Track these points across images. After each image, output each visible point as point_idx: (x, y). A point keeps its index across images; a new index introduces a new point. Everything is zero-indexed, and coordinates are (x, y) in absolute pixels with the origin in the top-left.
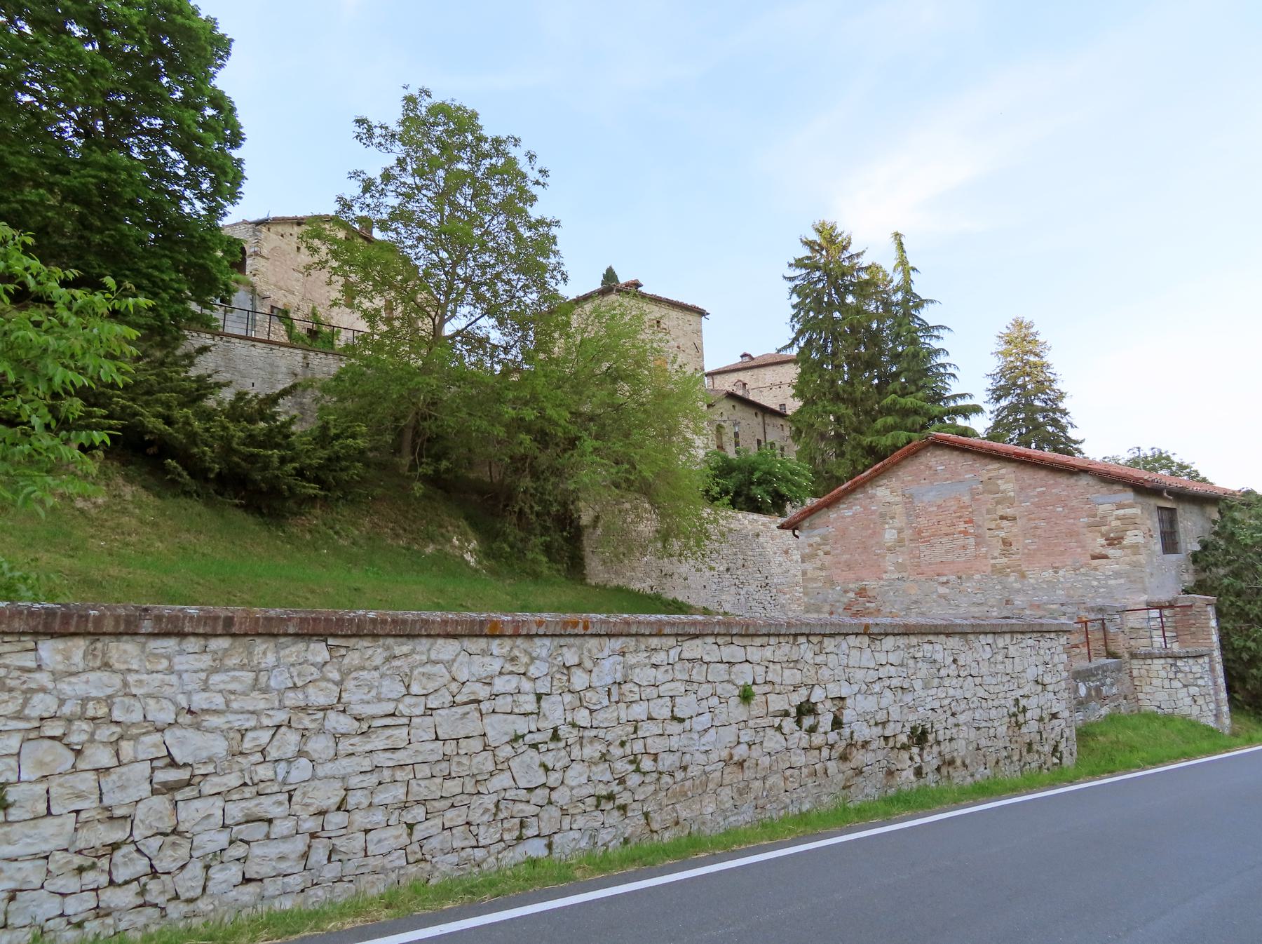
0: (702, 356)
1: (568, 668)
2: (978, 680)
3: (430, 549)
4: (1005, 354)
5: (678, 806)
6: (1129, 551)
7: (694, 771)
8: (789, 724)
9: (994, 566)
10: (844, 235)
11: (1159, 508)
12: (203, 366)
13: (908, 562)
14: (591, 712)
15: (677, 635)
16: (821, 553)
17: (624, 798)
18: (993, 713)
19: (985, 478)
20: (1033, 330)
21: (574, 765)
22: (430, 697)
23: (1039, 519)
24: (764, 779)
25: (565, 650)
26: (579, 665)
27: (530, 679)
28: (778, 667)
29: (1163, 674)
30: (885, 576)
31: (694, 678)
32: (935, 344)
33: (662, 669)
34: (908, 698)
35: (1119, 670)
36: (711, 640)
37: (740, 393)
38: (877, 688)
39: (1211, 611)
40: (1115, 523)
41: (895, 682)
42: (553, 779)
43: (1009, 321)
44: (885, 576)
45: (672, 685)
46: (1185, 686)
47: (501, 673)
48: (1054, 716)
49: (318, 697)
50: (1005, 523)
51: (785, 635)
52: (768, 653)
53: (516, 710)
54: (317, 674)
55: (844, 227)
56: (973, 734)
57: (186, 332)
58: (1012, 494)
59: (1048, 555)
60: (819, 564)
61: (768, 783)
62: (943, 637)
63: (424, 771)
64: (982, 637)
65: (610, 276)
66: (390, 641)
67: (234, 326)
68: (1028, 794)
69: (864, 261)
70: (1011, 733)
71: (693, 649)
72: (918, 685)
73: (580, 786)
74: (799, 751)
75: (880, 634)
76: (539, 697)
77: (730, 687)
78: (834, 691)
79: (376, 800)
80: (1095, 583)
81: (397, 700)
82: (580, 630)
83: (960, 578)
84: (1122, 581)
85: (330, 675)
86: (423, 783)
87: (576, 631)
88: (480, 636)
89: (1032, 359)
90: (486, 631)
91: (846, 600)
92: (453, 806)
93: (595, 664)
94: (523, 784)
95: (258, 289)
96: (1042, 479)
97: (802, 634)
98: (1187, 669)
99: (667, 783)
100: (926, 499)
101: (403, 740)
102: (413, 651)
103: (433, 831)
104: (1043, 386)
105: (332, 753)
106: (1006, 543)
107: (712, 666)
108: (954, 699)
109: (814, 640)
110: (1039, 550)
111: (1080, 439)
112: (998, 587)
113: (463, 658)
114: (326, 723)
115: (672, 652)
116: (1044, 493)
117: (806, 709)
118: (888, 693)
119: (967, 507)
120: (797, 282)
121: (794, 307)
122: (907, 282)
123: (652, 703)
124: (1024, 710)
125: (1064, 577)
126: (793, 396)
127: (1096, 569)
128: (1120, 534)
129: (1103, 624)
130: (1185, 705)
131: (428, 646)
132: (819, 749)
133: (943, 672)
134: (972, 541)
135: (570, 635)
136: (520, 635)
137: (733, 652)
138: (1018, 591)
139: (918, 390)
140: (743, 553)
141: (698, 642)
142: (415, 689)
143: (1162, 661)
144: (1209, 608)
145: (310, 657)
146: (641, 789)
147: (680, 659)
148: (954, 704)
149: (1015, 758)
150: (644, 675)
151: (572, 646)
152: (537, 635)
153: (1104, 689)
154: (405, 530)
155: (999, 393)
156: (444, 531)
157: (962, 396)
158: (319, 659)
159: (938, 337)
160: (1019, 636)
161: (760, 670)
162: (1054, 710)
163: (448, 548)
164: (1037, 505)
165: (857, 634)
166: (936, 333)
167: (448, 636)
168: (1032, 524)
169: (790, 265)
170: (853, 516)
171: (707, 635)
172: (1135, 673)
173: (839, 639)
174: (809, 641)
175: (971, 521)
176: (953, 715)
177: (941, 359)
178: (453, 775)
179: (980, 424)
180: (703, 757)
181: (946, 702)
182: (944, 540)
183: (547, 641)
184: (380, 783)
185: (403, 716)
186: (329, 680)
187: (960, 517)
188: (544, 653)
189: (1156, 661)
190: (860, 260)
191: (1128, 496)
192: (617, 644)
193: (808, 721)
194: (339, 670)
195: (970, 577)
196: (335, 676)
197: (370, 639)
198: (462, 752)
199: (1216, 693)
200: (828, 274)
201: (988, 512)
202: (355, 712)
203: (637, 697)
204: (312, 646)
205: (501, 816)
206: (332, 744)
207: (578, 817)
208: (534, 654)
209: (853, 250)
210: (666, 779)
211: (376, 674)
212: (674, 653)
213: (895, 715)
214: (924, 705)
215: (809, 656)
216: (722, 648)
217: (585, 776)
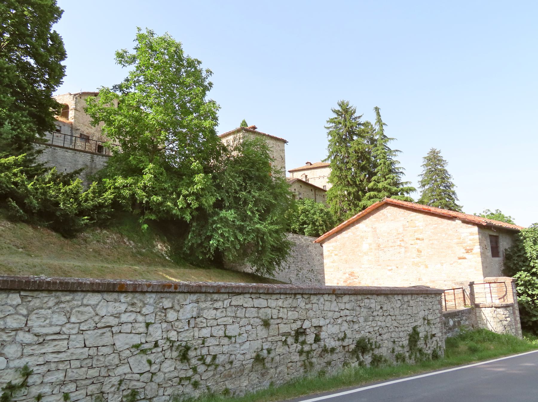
0: (284, 161)
1: (166, 309)
2: (393, 318)
4: (426, 165)
5: (226, 382)
7: (237, 364)
8: (290, 340)
10: (352, 108)
11: (490, 236)
12: (41, 159)
14: (178, 333)
15: (228, 293)
16: (333, 255)
17: (197, 377)
18: (402, 334)
21: (166, 361)
22: (82, 324)
24: (276, 368)
25: (164, 300)
26: (172, 308)
27: (143, 315)
28: (285, 310)
31: (238, 315)
32: (394, 159)
33: (220, 311)
34: (356, 327)
36: (248, 296)
37: (304, 180)
41: (349, 318)
42: (154, 368)
45: (225, 319)
47: (125, 311)
48: (434, 335)
49: (12, 323)
50: (418, 241)
51: (289, 294)
52: (280, 303)
53: (134, 331)
54: (12, 311)
55: (352, 104)
58: (421, 228)
61: (279, 370)
62: (375, 296)
63: (77, 364)
64: (395, 296)
65: (244, 123)
66: (59, 294)
68: (468, 364)
69: (362, 120)
71: (237, 300)
72: (361, 320)
73: (169, 372)
74: (296, 354)
75: (341, 294)
76: (148, 325)
77: (258, 320)
78: (316, 322)
79: (46, 380)
81: (62, 326)
82: (172, 289)
85: (21, 311)
86: (75, 371)
87: (170, 290)
88: (113, 292)
90: (117, 289)
92: (93, 383)
93: (181, 307)
94: (136, 371)
97: (299, 294)
99: (221, 370)
101: (64, 347)
102: (73, 299)
103: (79, 397)
105: (19, 354)
106: (419, 251)
107: (248, 309)
108: (380, 327)
109: (306, 296)
111: (461, 205)
113: (103, 303)
114: (17, 338)
115: (226, 302)
117: (300, 333)
118: (345, 324)
120: (331, 130)
123: (213, 328)
126: (328, 182)
127: (460, 264)
131: (82, 297)
133: (375, 314)
134: (403, 250)
135: (167, 292)
136: (137, 292)
137: (261, 302)
140: (301, 255)
141: (241, 297)
142: (73, 319)
145: (9, 302)
146: (205, 374)
147: (230, 305)
148: (380, 329)
150: (210, 314)
151: (168, 298)
152: (147, 292)
153: (462, 322)
157: (406, 183)
158: (15, 303)
160: (416, 296)
161: (275, 311)
162: (433, 333)
165: (329, 294)
166: (394, 154)
167: (94, 291)
168: (431, 242)
169: (328, 122)
171: (246, 293)
173: (319, 296)
174: (303, 297)
175: (403, 240)
176: (380, 335)
178: (94, 366)
179: (416, 196)
180: (242, 356)
181: (377, 328)
183: (154, 295)
184: (49, 371)
185: (65, 334)
186: (20, 314)
187: (398, 238)
188: (152, 301)
192: (194, 297)
193: (301, 339)
194: (27, 309)
196: (25, 312)
197: (47, 292)
198: (100, 354)
199: (515, 325)
202: (35, 332)
203: (205, 325)
204: (11, 295)
205: (122, 388)
206: (20, 349)
207: (168, 389)
208: (146, 302)
209: (356, 115)
210: (221, 368)
211: (50, 311)
212: (227, 303)
213: (349, 335)
214: (365, 330)
215: (302, 305)
216: (254, 300)
217: (173, 367)
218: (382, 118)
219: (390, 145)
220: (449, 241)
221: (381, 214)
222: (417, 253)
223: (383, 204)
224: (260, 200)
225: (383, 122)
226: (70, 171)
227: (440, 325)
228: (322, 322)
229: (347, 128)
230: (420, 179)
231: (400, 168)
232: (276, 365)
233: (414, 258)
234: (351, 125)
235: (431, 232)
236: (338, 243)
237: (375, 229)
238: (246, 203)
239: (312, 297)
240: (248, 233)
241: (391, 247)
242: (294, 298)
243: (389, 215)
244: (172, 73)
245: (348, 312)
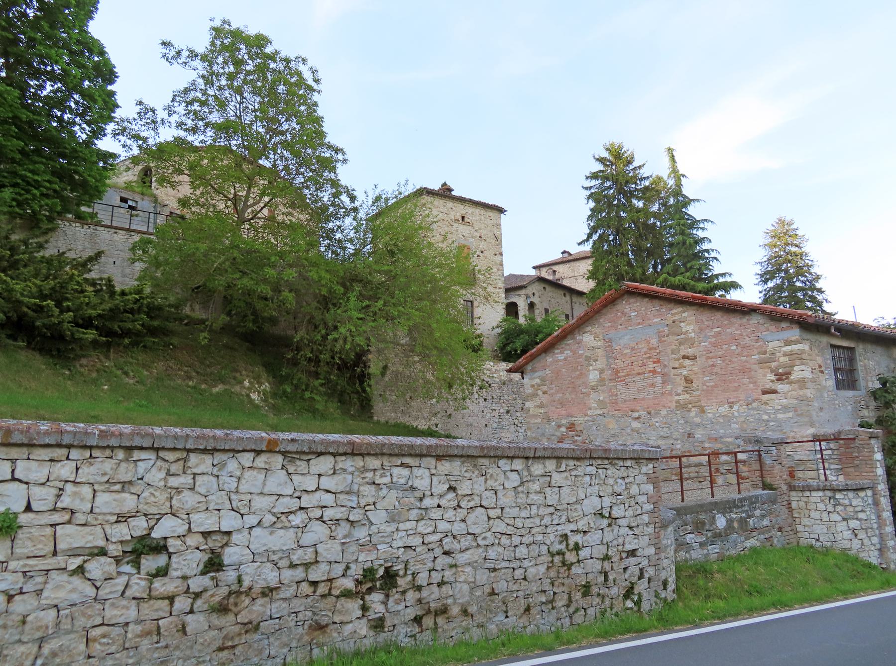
0: (500, 244)
3: (218, 389)
4: (772, 246)
6: (796, 386)
9: (677, 402)
10: (629, 153)
11: (833, 346)
13: (607, 400)
16: (540, 393)
19: (670, 322)
20: (793, 227)
23: (716, 357)
29: (821, 506)
30: (589, 412)
32: (701, 234)
34: (361, 533)
35: (774, 502)
38: (297, 519)
39: (876, 444)
40: (783, 359)
41: (328, 514)
43: (773, 220)
44: (589, 412)
46: (844, 519)
50: (687, 362)
52: (65, 470)
55: (628, 147)
56: (483, 577)
57: (60, 222)
58: (693, 335)
59: (724, 391)
60: (538, 402)
64: (502, 462)
67: (104, 216)
70: (553, 574)
78: (204, 521)
80: (765, 417)
83: (649, 413)
84: (790, 415)
89: (793, 249)
91: (559, 434)
95: (160, 199)
96: (718, 320)
98: (847, 502)
100: (622, 342)
104: (801, 271)
106: (688, 380)
110: (716, 386)
111: (834, 312)
112: (682, 421)
116: (719, 332)
119: (655, 349)
120: (593, 191)
121: (591, 210)
122: (679, 185)
124: (577, 547)
125: (738, 411)
127: (766, 403)
128: (787, 370)
129: (760, 455)
130: (844, 538)
132: (171, 599)
134: (659, 379)
138: (698, 425)
139: (687, 271)
143: (821, 494)
144: (873, 441)
149: (560, 602)
153: (751, 521)
154: (198, 373)
155: (766, 277)
156: (238, 375)
157: (723, 275)
159: (703, 229)
160: (571, 463)
162: (629, 547)
163: (237, 389)
164: (714, 345)
166: (701, 225)
168: (710, 362)
169: (587, 178)
170: (565, 360)
172: (794, 505)
173: (219, 457)
175: (659, 361)
176: (446, 553)
177: (705, 246)
182: (637, 378)
187: (649, 358)
189: (814, 494)
190: (642, 171)
191: (795, 333)
195: (658, 413)
200: (615, 182)
201: (673, 353)
209: (635, 164)
214: (390, 539)
215: (156, 476)
220: (744, 358)
222: (685, 384)
226: (86, 255)
227: (650, 530)
228: (229, 522)
230: (758, 269)
231: (713, 250)
232: (39, 634)
233: (679, 395)
235: (710, 343)
236: (548, 372)
239: (194, 458)
241: (639, 374)
242: (127, 460)
244: (259, 86)
245: (328, 499)
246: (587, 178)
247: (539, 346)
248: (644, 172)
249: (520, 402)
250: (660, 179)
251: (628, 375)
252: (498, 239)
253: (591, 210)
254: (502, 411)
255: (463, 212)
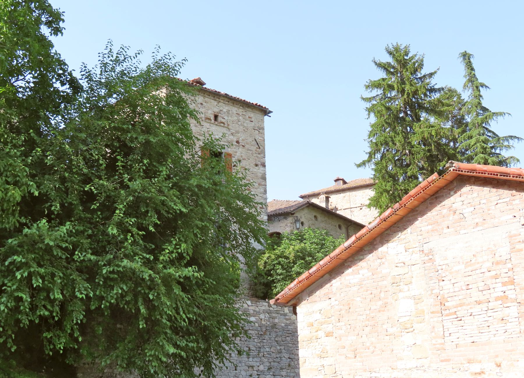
0: (263, 152)
166: (506, 143)
182: (476, 310)
187: (496, 277)
209: (424, 71)
218: (477, 73)
219: (494, 126)
221: (445, 211)
223: (451, 182)
224: (146, 201)
225: (480, 81)
229: (405, 96)
234: (413, 89)
237: (429, 256)
238: (108, 208)
240: (109, 283)
241: (479, 303)
243: (467, 211)
246: (367, 87)
247: (321, 263)
248: (437, 82)
249: (287, 356)
250: (452, 92)
251: (461, 305)
252: (260, 147)
253: (372, 126)
254: (261, 368)
255: (216, 110)
